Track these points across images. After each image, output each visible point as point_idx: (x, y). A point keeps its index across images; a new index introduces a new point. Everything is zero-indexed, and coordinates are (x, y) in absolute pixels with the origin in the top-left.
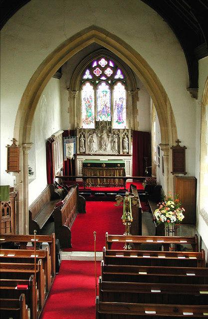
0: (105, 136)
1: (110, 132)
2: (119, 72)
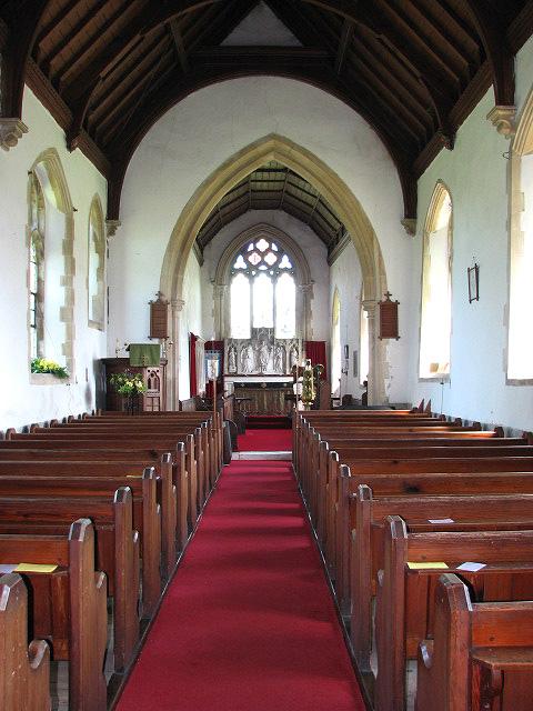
0: (264, 349)
1: (272, 343)
2: (285, 259)
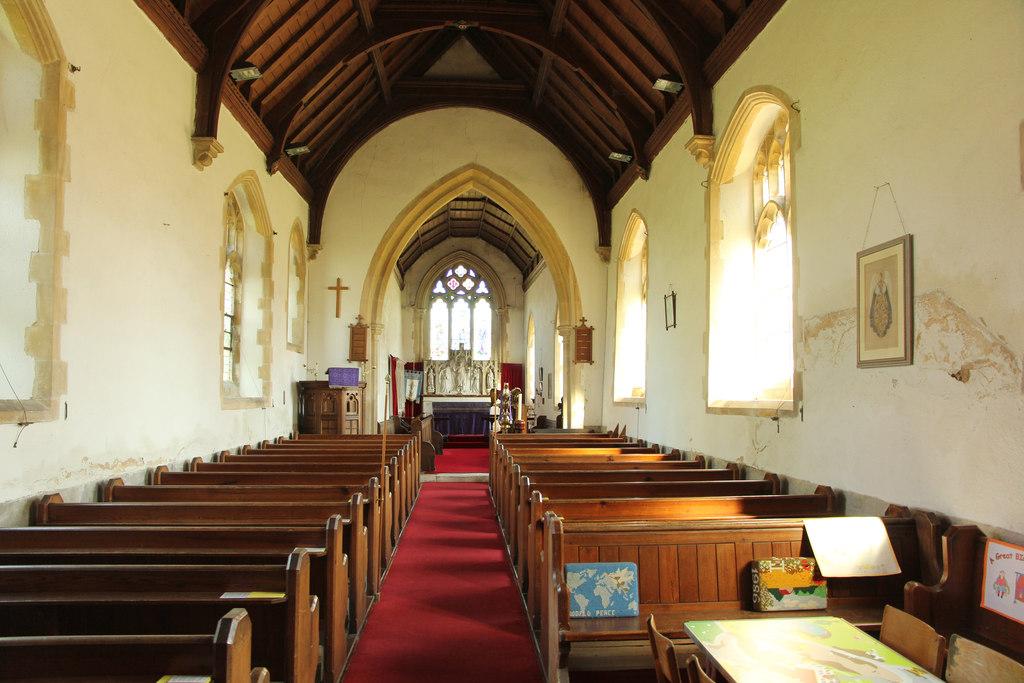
0: (462, 370)
1: (470, 365)
2: (482, 284)
